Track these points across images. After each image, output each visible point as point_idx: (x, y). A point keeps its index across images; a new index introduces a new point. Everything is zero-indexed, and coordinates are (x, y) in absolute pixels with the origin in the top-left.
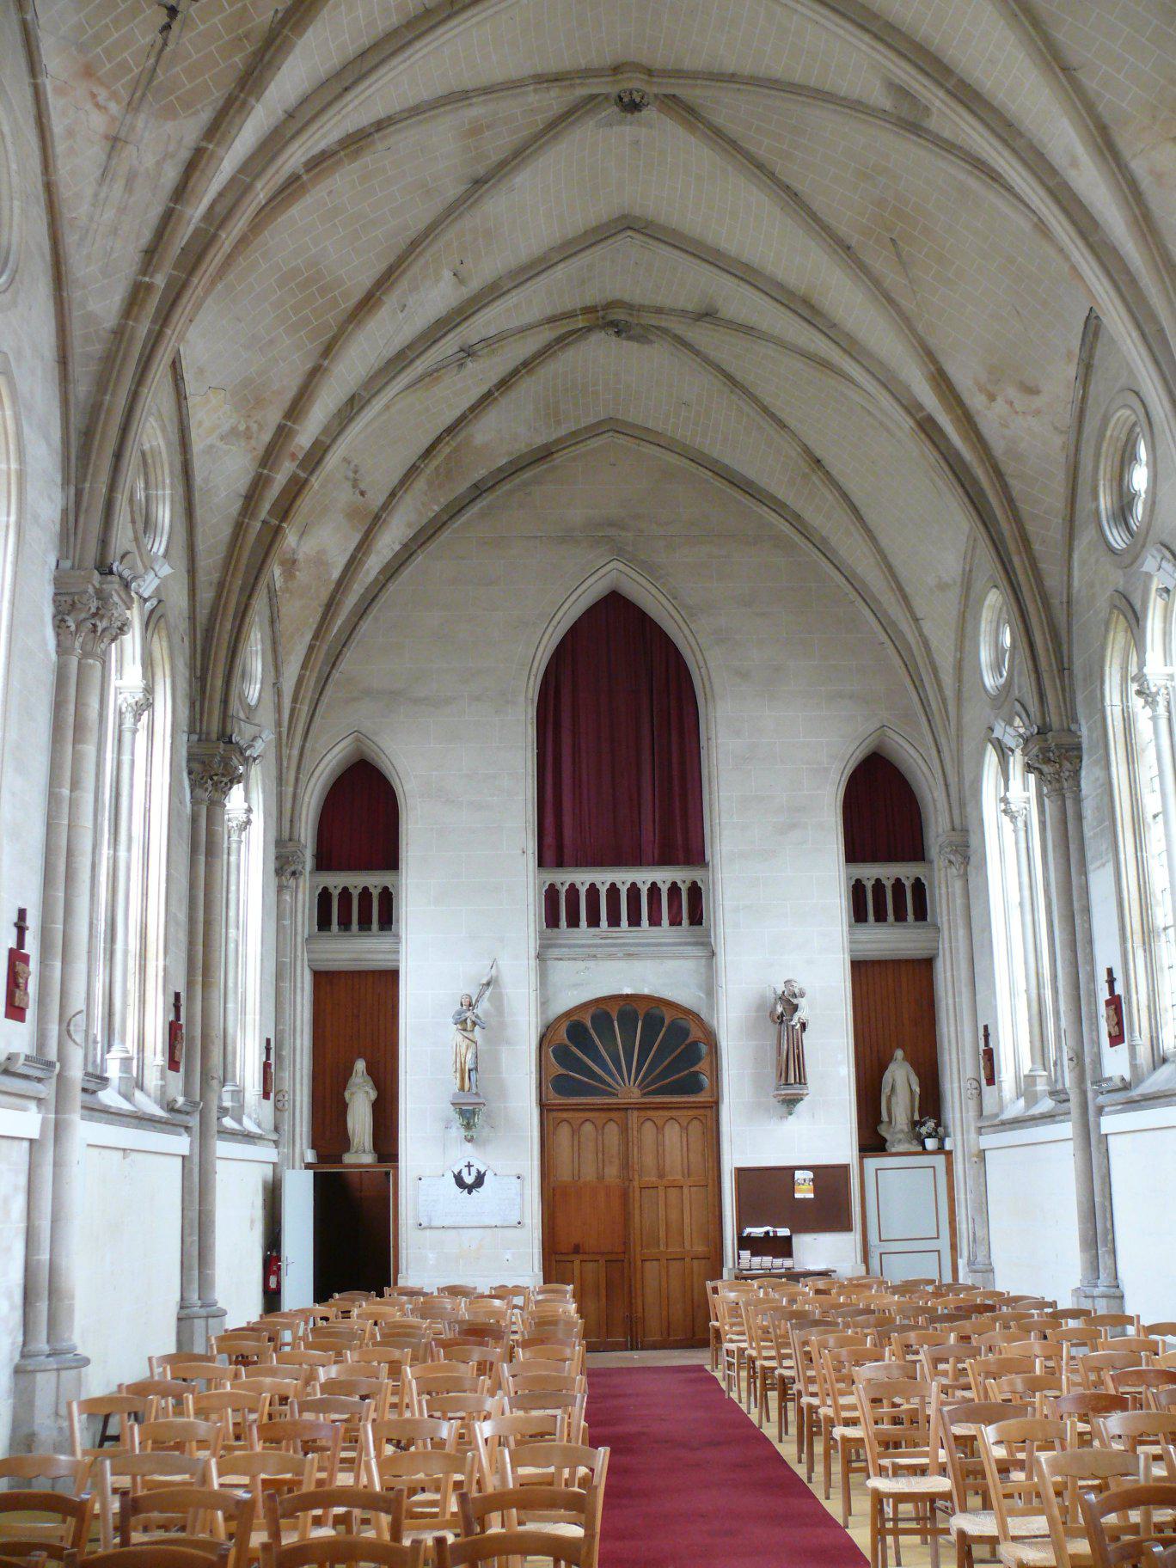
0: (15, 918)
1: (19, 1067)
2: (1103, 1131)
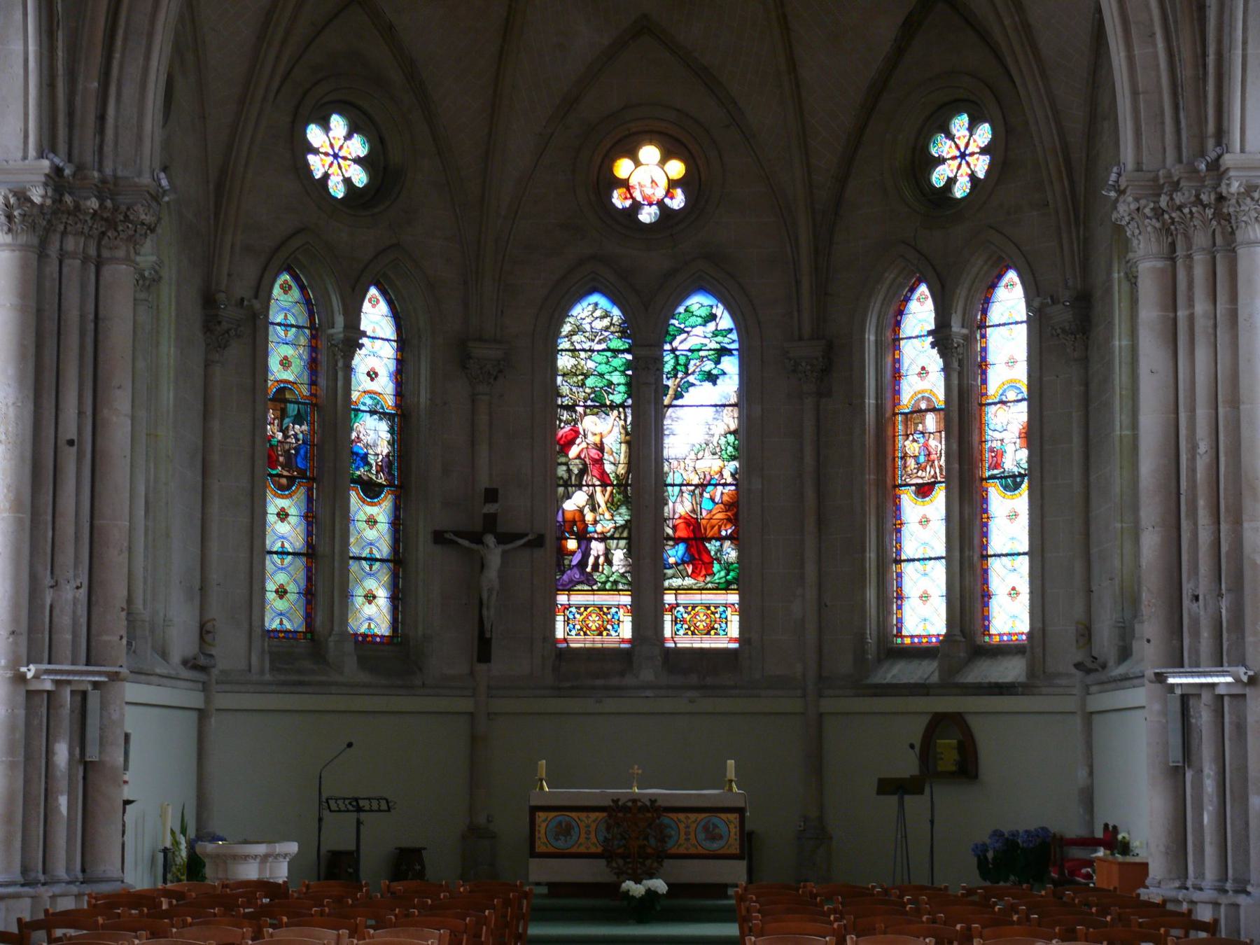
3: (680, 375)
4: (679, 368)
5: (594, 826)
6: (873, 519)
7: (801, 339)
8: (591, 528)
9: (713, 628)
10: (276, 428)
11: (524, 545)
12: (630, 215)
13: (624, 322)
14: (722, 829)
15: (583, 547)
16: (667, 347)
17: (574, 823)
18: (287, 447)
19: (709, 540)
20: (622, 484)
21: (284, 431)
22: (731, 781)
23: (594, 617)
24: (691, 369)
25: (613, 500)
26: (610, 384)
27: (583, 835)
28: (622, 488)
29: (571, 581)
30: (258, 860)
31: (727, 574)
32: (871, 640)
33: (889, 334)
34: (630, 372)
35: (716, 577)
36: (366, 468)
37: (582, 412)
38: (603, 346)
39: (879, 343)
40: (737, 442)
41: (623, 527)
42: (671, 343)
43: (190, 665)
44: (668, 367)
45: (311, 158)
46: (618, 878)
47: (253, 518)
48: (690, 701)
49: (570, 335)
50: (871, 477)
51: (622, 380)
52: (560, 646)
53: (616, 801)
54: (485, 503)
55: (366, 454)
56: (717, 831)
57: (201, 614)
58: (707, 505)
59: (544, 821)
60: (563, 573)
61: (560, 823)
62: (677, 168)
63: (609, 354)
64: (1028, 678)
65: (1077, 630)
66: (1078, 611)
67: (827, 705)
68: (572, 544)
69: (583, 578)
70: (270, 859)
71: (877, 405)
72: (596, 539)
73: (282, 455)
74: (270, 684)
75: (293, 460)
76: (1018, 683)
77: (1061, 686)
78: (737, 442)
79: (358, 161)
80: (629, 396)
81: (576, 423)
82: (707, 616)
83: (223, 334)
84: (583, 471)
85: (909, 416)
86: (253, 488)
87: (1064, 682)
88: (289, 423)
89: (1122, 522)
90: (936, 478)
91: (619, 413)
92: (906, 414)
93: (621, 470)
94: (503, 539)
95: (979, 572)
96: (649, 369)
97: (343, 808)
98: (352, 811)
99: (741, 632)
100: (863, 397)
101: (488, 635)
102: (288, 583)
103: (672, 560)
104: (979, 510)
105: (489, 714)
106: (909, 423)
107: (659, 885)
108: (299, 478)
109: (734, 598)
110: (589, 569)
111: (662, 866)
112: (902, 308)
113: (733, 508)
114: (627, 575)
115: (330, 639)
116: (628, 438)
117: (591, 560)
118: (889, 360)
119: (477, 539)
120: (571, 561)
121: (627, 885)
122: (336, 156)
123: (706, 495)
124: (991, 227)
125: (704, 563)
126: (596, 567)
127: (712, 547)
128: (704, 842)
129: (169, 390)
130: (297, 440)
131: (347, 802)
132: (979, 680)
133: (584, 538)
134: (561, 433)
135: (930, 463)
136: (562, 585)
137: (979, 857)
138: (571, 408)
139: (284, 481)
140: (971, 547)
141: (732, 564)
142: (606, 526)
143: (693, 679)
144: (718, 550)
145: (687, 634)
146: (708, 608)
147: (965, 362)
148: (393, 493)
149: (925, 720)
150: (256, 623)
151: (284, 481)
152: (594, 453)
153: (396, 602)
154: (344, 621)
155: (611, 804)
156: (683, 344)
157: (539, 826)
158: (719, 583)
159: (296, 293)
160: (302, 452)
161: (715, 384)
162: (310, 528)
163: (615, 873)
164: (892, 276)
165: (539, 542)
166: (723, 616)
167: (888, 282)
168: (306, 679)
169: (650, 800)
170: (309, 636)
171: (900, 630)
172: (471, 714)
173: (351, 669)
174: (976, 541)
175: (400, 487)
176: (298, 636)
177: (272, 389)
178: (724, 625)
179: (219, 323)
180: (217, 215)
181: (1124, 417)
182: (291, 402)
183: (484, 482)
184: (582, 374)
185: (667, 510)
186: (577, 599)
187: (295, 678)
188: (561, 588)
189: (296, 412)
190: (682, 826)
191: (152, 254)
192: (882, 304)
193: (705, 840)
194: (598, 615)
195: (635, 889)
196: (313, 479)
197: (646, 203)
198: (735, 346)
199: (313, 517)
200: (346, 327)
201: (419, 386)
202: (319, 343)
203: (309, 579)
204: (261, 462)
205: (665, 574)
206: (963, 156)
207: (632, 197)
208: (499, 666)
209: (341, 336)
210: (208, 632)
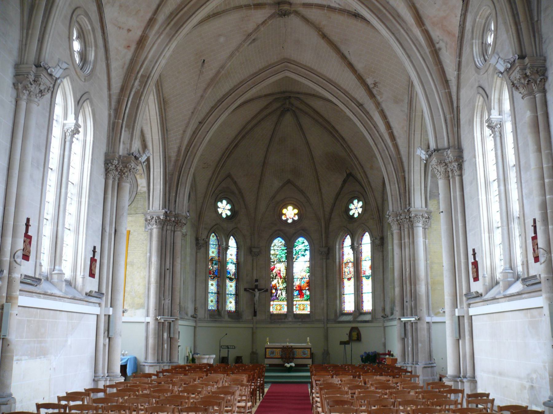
0: (93, 249)
1: (93, 294)
2: (470, 314)
3: (297, 255)
7: (323, 247)
8: (278, 288)
11: (264, 291)
14: (306, 352)
16: (294, 249)
19: (303, 290)
20: (284, 278)
21: (213, 267)
24: (299, 254)
26: (282, 257)
32: (338, 311)
39: (339, 248)
41: (285, 287)
49: (273, 246)
53: (283, 346)
62: (296, 211)
67: (329, 325)
68: (274, 291)
74: (210, 321)
84: (276, 275)
93: (285, 275)
94: (259, 290)
100: (336, 259)
103: (295, 295)
109: (309, 302)
110: (277, 296)
113: (308, 283)
117: (278, 295)
118: (341, 251)
119: (254, 290)
123: (303, 280)
126: (279, 296)
127: (304, 291)
133: (276, 290)
134: (271, 267)
140: (359, 291)
142: (281, 287)
143: (300, 320)
149: (349, 329)
150: (206, 308)
154: (225, 307)
156: (297, 248)
159: (215, 237)
165: (267, 291)
171: (344, 309)
173: (226, 318)
174: (360, 290)
180: (199, 221)
183: (255, 278)
185: (294, 284)
187: (215, 320)
190: (298, 352)
195: (288, 365)
198: (309, 249)
203: (218, 298)
208: (258, 317)
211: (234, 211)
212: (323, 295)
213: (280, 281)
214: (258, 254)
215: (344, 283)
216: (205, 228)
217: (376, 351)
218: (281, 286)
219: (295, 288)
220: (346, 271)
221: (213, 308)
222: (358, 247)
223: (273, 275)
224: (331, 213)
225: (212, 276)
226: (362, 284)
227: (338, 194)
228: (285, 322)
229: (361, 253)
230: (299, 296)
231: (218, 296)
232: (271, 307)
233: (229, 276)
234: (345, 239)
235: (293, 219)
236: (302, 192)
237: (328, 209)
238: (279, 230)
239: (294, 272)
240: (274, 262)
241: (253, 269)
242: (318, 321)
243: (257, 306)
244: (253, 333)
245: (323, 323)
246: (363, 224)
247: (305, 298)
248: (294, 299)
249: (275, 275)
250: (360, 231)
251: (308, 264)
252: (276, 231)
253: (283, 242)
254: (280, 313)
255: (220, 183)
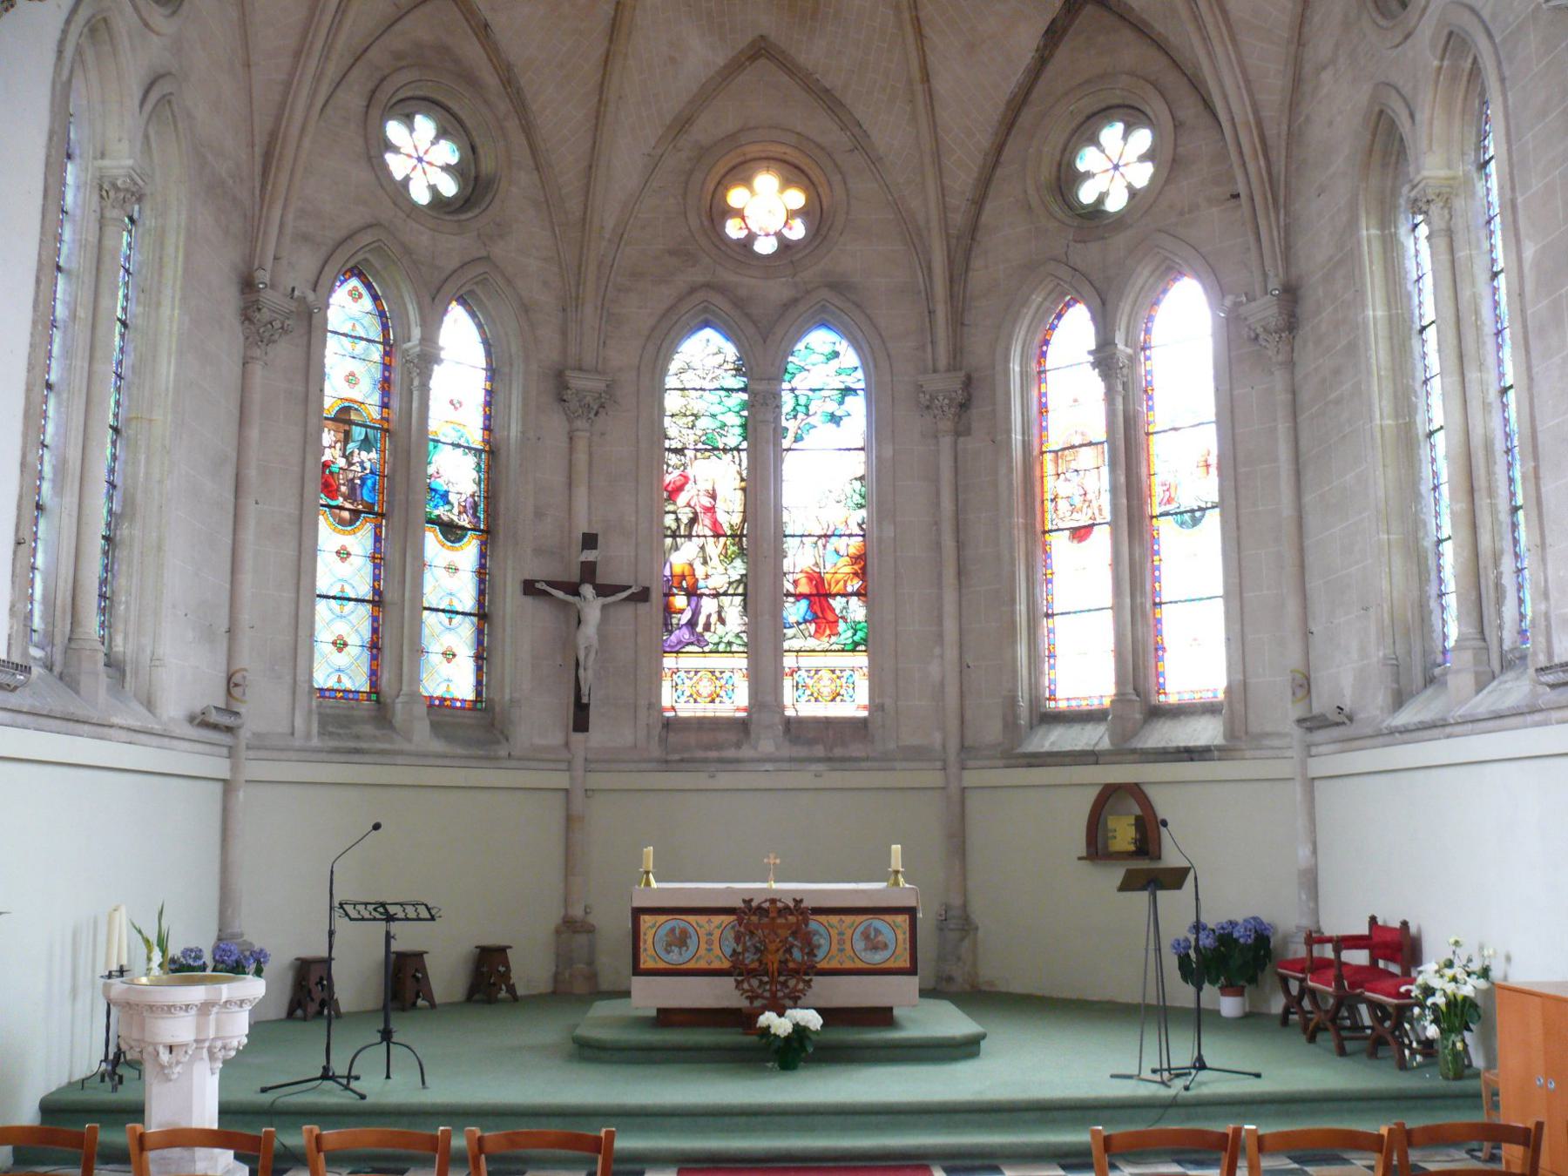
3: (801, 416)
4: (798, 408)
5: (717, 933)
6: (1023, 568)
7: (935, 371)
8: (701, 583)
9: (839, 694)
10: (337, 453)
11: (628, 599)
12: (745, 246)
13: (739, 359)
14: (887, 934)
15: (693, 604)
16: (785, 385)
17: (691, 930)
18: (351, 476)
19: (834, 596)
20: (737, 536)
21: (347, 457)
22: (897, 872)
23: (705, 682)
24: (812, 410)
25: (726, 553)
26: (724, 426)
27: (703, 946)
28: (737, 539)
29: (680, 642)
30: (193, 1012)
31: (855, 634)
32: (1023, 704)
33: (1034, 366)
34: (745, 413)
35: (843, 637)
36: (447, 507)
37: (693, 457)
38: (716, 384)
39: (1024, 375)
40: (863, 489)
41: (739, 582)
42: (790, 382)
43: (198, 721)
44: (787, 407)
45: (389, 157)
46: (751, 1003)
47: (300, 552)
48: (816, 776)
49: (682, 371)
50: (1019, 520)
51: (738, 421)
52: (667, 714)
53: (748, 902)
54: (583, 549)
55: (447, 492)
56: (880, 938)
57: (229, 664)
58: (831, 558)
59: (651, 927)
60: (671, 632)
61: (673, 930)
62: (796, 198)
63: (723, 393)
64: (1225, 737)
65: (1294, 679)
66: (1293, 657)
67: (971, 778)
68: (680, 601)
69: (693, 639)
70: (215, 1010)
71: (1024, 441)
72: (708, 595)
73: (344, 484)
74: (320, 751)
75: (358, 492)
76: (1216, 746)
77: (1272, 748)
78: (863, 489)
79: (447, 168)
80: (745, 439)
81: (685, 468)
82: (832, 680)
83: (265, 325)
84: (694, 521)
85: (1060, 453)
86: (301, 516)
87: (1276, 742)
88: (354, 448)
89: (1388, 533)
90: (1095, 519)
91: (734, 457)
92: (1056, 452)
93: (737, 519)
94: (603, 591)
95: (1151, 622)
96: (767, 405)
97: (367, 915)
98: (379, 920)
99: (871, 698)
100: (1008, 432)
101: (585, 700)
102: (349, 634)
103: (792, 619)
104: (1149, 552)
105: (586, 790)
106: (1060, 461)
107: (813, 1020)
108: (364, 512)
109: (861, 660)
110: (699, 629)
111: (810, 987)
112: (1048, 337)
113: (861, 563)
114: (741, 635)
115: (397, 701)
116: (743, 484)
117: (702, 620)
118: (1035, 394)
119: (573, 590)
120: (679, 620)
121: (768, 1018)
122: (420, 160)
123: (830, 547)
124: (1159, 231)
125: (828, 622)
126: (707, 627)
127: (838, 603)
128: (863, 954)
129: (169, 362)
130: (364, 468)
131: (370, 908)
132: (1162, 744)
133: (693, 593)
134: (668, 478)
135: (1087, 504)
136: (669, 646)
137: (1180, 957)
138: (679, 451)
139: (346, 515)
140: (1143, 593)
141: (859, 623)
142: (718, 581)
143: (819, 751)
144: (844, 608)
145: (809, 701)
146: (833, 672)
147: (1130, 386)
148: (478, 537)
149: (1091, 795)
150: (301, 678)
151: (346, 515)
152: (707, 502)
153: (480, 662)
154: (415, 679)
155: (742, 905)
156: (801, 382)
157: (645, 934)
158: (845, 644)
159: (367, 303)
160: (369, 483)
161: (838, 424)
162: (377, 572)
163: (747, 997)
164: (1040, 299)
165: (643, 596)
166: (851, 680)
167: (1034, 306)
168: (364, 745)
169: (795, 900)
170: (374, 697)
171: (1052, 693)
172: (567, 791)
173: (422, 735)
174: (1148, 588)
175: (487, 532)
176: (361, 696)
177: (330, 405)
178: (850, 690)
179: (259, 310)
180: (263, 187)
181: (1384, 403)
182: (357, 425)
183: (582, 527)
184: (693, 415)
185: (787, 564)
186: (686, 662)
187: (352, 744)
188: (668, 649)
189: (363, 437)
190: (834, 932)
191: (130, 158)
192: (1028, 332)
193: (865, 950)
194: (711, 680)
195: (780, 1024)
196: (382, 515)
197: (762, 233)
198: (862, 385)
199: (381, 559)
200: (423, 340)
201: (509, 419)
202: (393, 360)
203: (375, 631)
204: (313, 484)
205: (785, 635)
206: (1116, 167)
207: (747, 228)
208: (598, 735)
209: (418, 349)
210: (236, 685)
211: (476, 178)
212: (940, 621)
213: (714, 548)
214: (599, 406)
215: (1047, 555)
216: (305, 238)
217: (1256, 914)
218: (720, 572)
219: (789, 587)
220: (1062, 493)
221: (347, 684)
222: (1133, 360)
223: (677, 520)
224: (979, 202)
225: (341, 508)
226: (1157, 553)
227: (1019, 103)
228: (737, 761)
229: (1147, 392)
230: (812, 627)
231: (375, 619)
232: (666, 686)
233: (441, 511)
234: (1053, 328)
235: (779, 235)
236: (829, 101)
237: (962, 180)
238: (708, 286)
239: (785, 501)
240: (679, 451)
241: (570, 485)
242: (918, 754)
243: (590, 673)
244: (570, 820)
245: (939, 764)
246: (1166, 232)
247: (845, 635)
248: (786, 645)
249: (685, 520)
250: (1146, 273)
251: (857, 464)
252: (693, 290)
253: (731, 351)
254: (710, 714)
255: (400, 18)
